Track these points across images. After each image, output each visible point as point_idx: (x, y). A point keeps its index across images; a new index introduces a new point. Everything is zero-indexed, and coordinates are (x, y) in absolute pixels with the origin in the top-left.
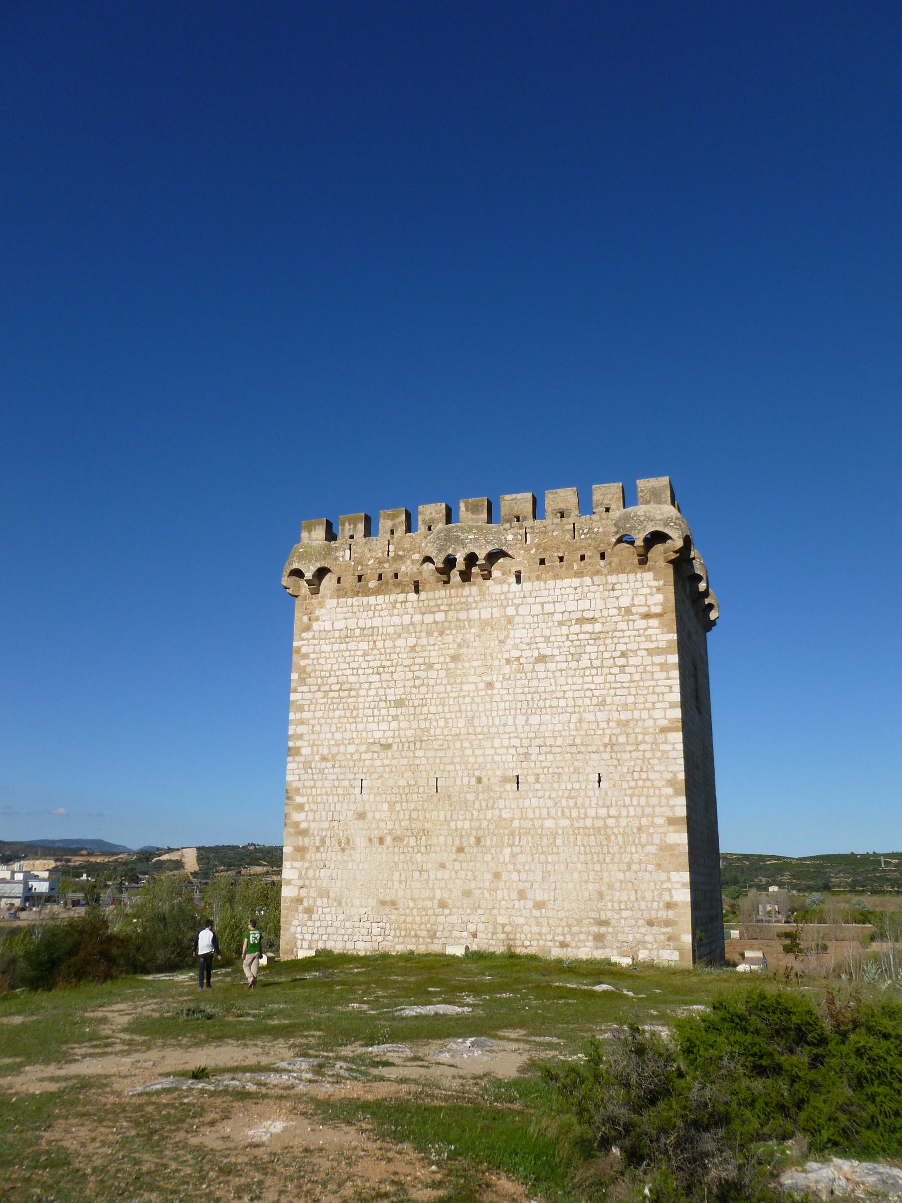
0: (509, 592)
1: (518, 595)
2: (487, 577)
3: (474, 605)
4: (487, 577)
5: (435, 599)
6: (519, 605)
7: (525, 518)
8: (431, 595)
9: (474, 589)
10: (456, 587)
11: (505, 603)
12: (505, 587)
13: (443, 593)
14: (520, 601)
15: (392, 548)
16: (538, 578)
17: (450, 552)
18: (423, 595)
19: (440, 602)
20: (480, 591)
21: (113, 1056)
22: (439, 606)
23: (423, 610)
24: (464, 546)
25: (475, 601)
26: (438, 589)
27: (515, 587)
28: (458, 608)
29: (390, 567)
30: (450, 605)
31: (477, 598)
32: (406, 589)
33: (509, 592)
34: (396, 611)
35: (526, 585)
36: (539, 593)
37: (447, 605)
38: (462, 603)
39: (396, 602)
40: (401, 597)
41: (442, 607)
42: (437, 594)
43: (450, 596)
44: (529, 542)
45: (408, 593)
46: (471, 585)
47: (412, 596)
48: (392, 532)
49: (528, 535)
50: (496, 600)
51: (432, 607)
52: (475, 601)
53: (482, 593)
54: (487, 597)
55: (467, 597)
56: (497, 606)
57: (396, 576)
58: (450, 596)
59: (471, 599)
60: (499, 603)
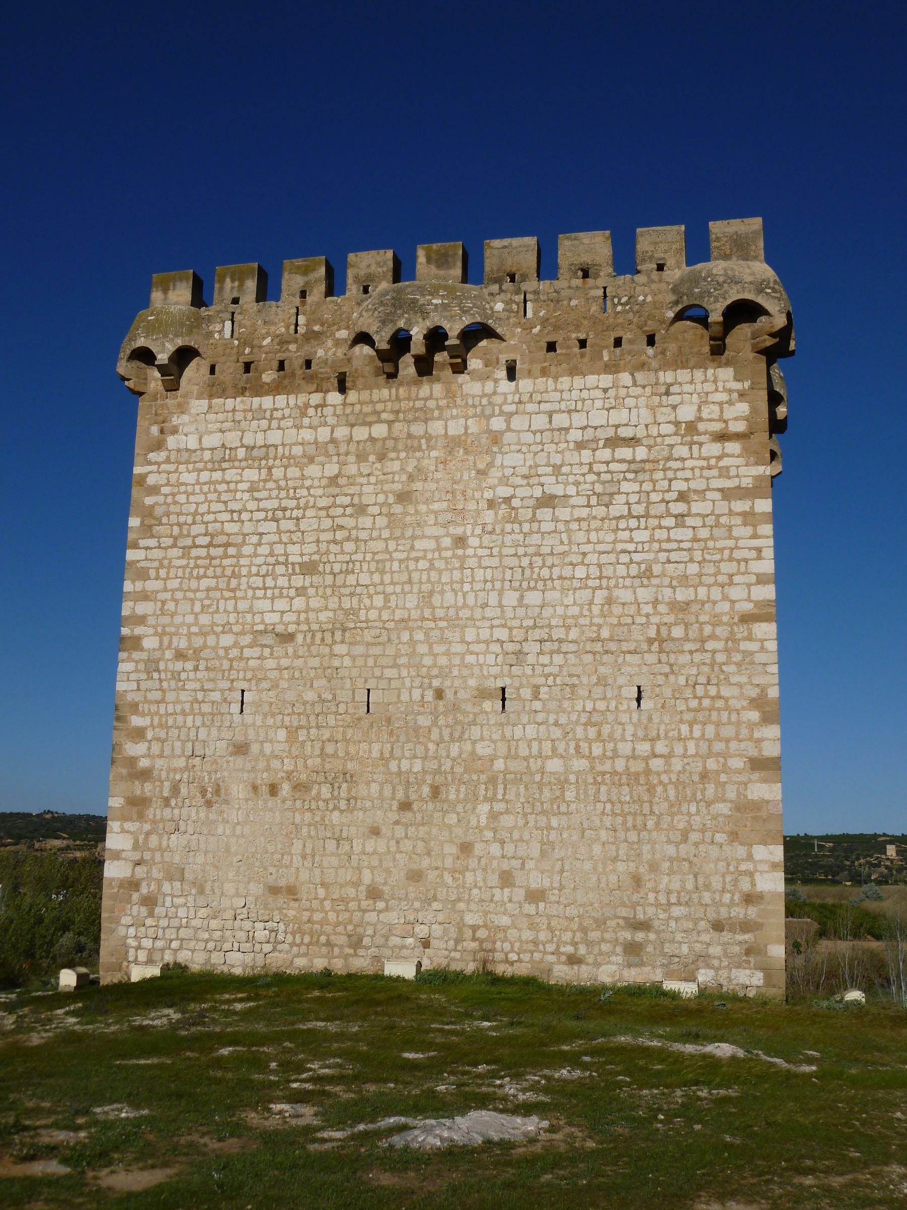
0: (495, 393)
1: (510, 398)
2: (460, 368)
4: (460, 368)
5: (372, 402)
7: (524, 278)
8: (365, 395)
9: (438, 388)
10: (407, 384)
11: (488, 412)
12: (489, 386)
13: (385, 392)
14: (513, 408)
15: (302, 319)
16: (544, 373)
17: (401, 324)
18: (352, 396)
19: (379, 407)
20: (448, 391)
22: (378, 413)
23: (352, 419)
26: (379, 387)
27: (506, 386)
29: (298, 350)
30: (397, 412)
31: (443, 403)
34: (306, 421)
35: (525, 384)
36: (546, 397)
37: (392, 412)
38: (417, 410)
39: (307, 405)
40: (316, 398)
41: (384, 416)
42: (376, 394)
44: (530, 314)
45: (327, 391)
46: (432, 382)
47: (334, 397)
48: (303, 294)
50: (474, 406)
51: (366, 414)
52: (438, 407)
53: (450, 395)
54: (459, 400)
57: (308, 364)
59: (431, 404)
60: (478, 410)
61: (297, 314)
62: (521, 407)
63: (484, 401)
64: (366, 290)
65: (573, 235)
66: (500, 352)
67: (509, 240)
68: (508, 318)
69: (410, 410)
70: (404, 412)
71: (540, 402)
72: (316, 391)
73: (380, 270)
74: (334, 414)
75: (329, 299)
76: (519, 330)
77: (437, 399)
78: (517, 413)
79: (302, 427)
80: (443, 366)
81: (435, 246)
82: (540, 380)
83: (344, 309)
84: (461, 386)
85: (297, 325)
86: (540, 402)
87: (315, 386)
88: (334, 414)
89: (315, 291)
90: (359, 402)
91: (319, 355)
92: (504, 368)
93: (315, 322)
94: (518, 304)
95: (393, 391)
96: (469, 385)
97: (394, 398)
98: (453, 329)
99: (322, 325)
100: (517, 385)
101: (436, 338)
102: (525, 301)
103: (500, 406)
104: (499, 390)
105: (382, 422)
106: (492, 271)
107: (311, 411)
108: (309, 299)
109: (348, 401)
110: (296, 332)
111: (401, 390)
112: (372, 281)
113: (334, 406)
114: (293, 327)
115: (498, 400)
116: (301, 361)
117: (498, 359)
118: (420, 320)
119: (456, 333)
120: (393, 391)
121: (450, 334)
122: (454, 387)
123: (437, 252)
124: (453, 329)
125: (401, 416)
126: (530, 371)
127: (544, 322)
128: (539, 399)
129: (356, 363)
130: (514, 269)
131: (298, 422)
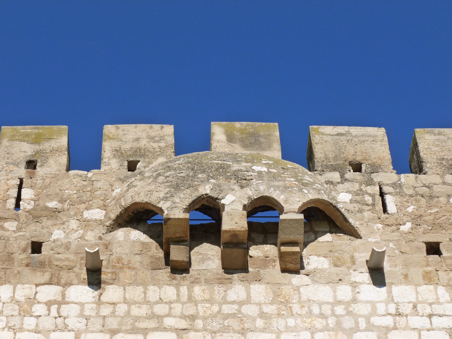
0: (354, 300)
1: (381, 308)
2: (292, 265)
3: (260, 323)
4: (292, 265)
5: (147, 302)
6: (388, 329)
7: (375, 169)
8: (135, 292)
9: (259, 291)
10: (207, 281)
11: (348, 323)
12: (344, 292)
13: (169, 292)
14: (389, 321)
15: (26, 193)
16: (428, 279)
17: (206, 189)
18: (111, 292)
19: (160, 309)
20: (277, 295)
21: (95, 333)
22: (160, 318)
23: (113, 323)
24: (243, 181)
25: (262, 315)
26: (157, 283)
27: (369, 291)
28: (215, 325)
29: (19, 229)
30: (193, 318)
31: (269, 309)
32: (65, 276)
33: (354, 300)
34: (30, 322)
35: (402, 292)
36: (437, 309)
37: (183, 317)
38: (227, 317)
39: (32, 300)
40: (50, 292)
41: (169, 322)
42: (153, 293)
43: (191, 299)
44: (391, 208)
45: (68, 284)
46: (249, 282)
47: (82, 293)
48: (31, 164)
49: (388, 198)
50: (322, 316)
51: (137, 319)
52: (262, 315)
53: (282, 301)
54: (296, 308)
55: (241, 303)
56: (326, 329)
57: (36, 247)
58: (191, 299)
59: (250, 310)
60: (331, 321)
61: (20, 187)
62: (402, 321)
63: (340, 310)
64: (132, 166)
65: (437, 130)
66: (355, 250)
67: (346, 128)
68: (361, 211)
69: (214, 316)
70: (205, 319)
71: (430, 316)
72: (50, 283)
73: (155, 145)
74: (81, 315)
75: (72, 172)
76: (380, 226)
77: (259, 304)
78: (395, 328)
79: (21, 330)
80: (265, 261)
81: (238, 125)
82: (424, 288)
83: (98, 185)
84: (297, 289)
85: (19, 199)
86: (430, 316)
87: (47, 276)
88: (81, 315)
89: (51, 161)
90: (125, 301)
91: (54, 237)
92: (365, 269)
93: (49, 197)
94: (373, 196)
95: (184, 290)
96: (310, 288)
97: (185, 298)
98: (292, 207)
99: (62, 201)
100: (390, 292)
101: (262, 210)
102: (382, 194)
103: (368, 318)
104: (361, 297)
105: (165, 329)
106: (326, 158)
107: (39, 309)
108: (40, 170)
109: (103, 298)
110: (17, 206)
111: (197, 289)
112: (143, 156)
113: (82, 305)
114: (13, 201)
115: (362, 309)
116: (25, 243)
117: (352, 257)
118: (236, 187)
119: (297, 206)
120: (184, 290)
121: (286, 207)
122: (286, 290)
123: (242, 131)
124: (292, 207)
125: (199, 323)
126: (406, 276)
127: (417, 220)
128: (428, 310)
129: (117, 250)
130: (359, 158)
131: (15, 321)
